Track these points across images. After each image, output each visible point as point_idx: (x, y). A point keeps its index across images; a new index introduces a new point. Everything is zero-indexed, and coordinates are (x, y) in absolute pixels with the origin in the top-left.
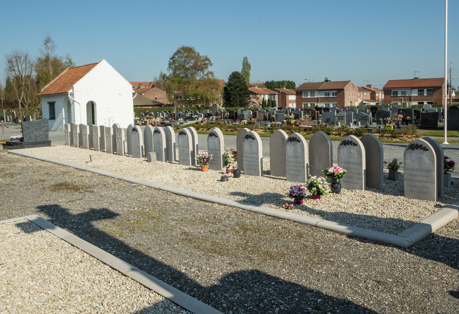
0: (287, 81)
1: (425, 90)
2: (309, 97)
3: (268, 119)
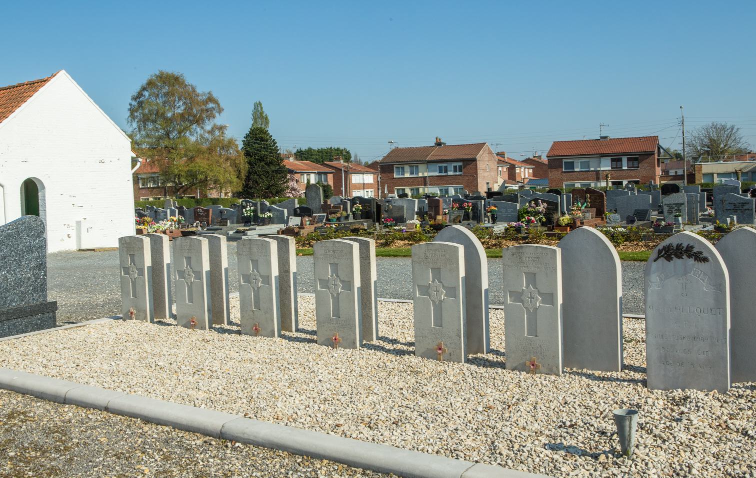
0: (336, 148)
1: (625, 159)
2: (407, 175)
3: (471, 215)
